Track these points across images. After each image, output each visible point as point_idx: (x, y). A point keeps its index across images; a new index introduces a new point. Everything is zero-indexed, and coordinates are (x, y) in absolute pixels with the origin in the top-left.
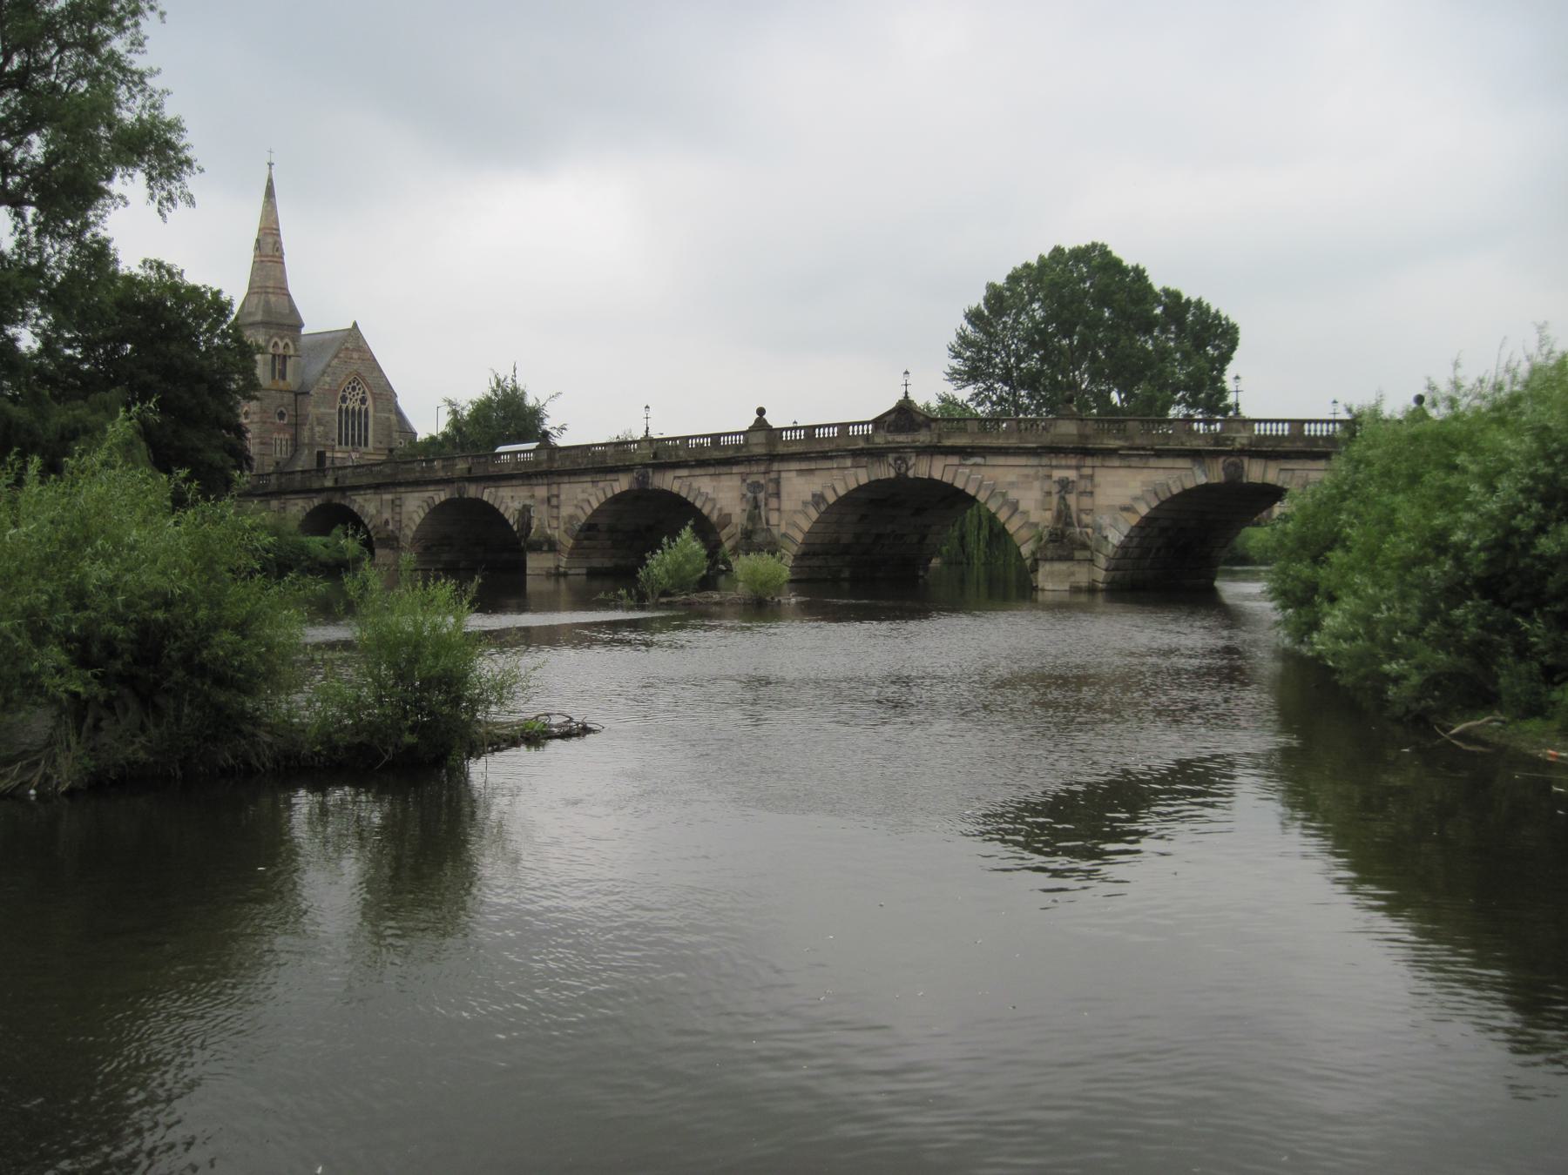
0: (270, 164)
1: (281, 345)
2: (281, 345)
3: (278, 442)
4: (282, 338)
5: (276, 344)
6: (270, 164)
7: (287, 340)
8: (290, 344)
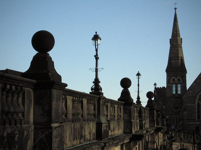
0: (175, 9)
1: (176, 79)
2: (176, 79)
3: (175, 119)
4: (176, 77)
5: (174, 80)
6: (175, 9)
7: (178, 77)
8: (181, 79)
